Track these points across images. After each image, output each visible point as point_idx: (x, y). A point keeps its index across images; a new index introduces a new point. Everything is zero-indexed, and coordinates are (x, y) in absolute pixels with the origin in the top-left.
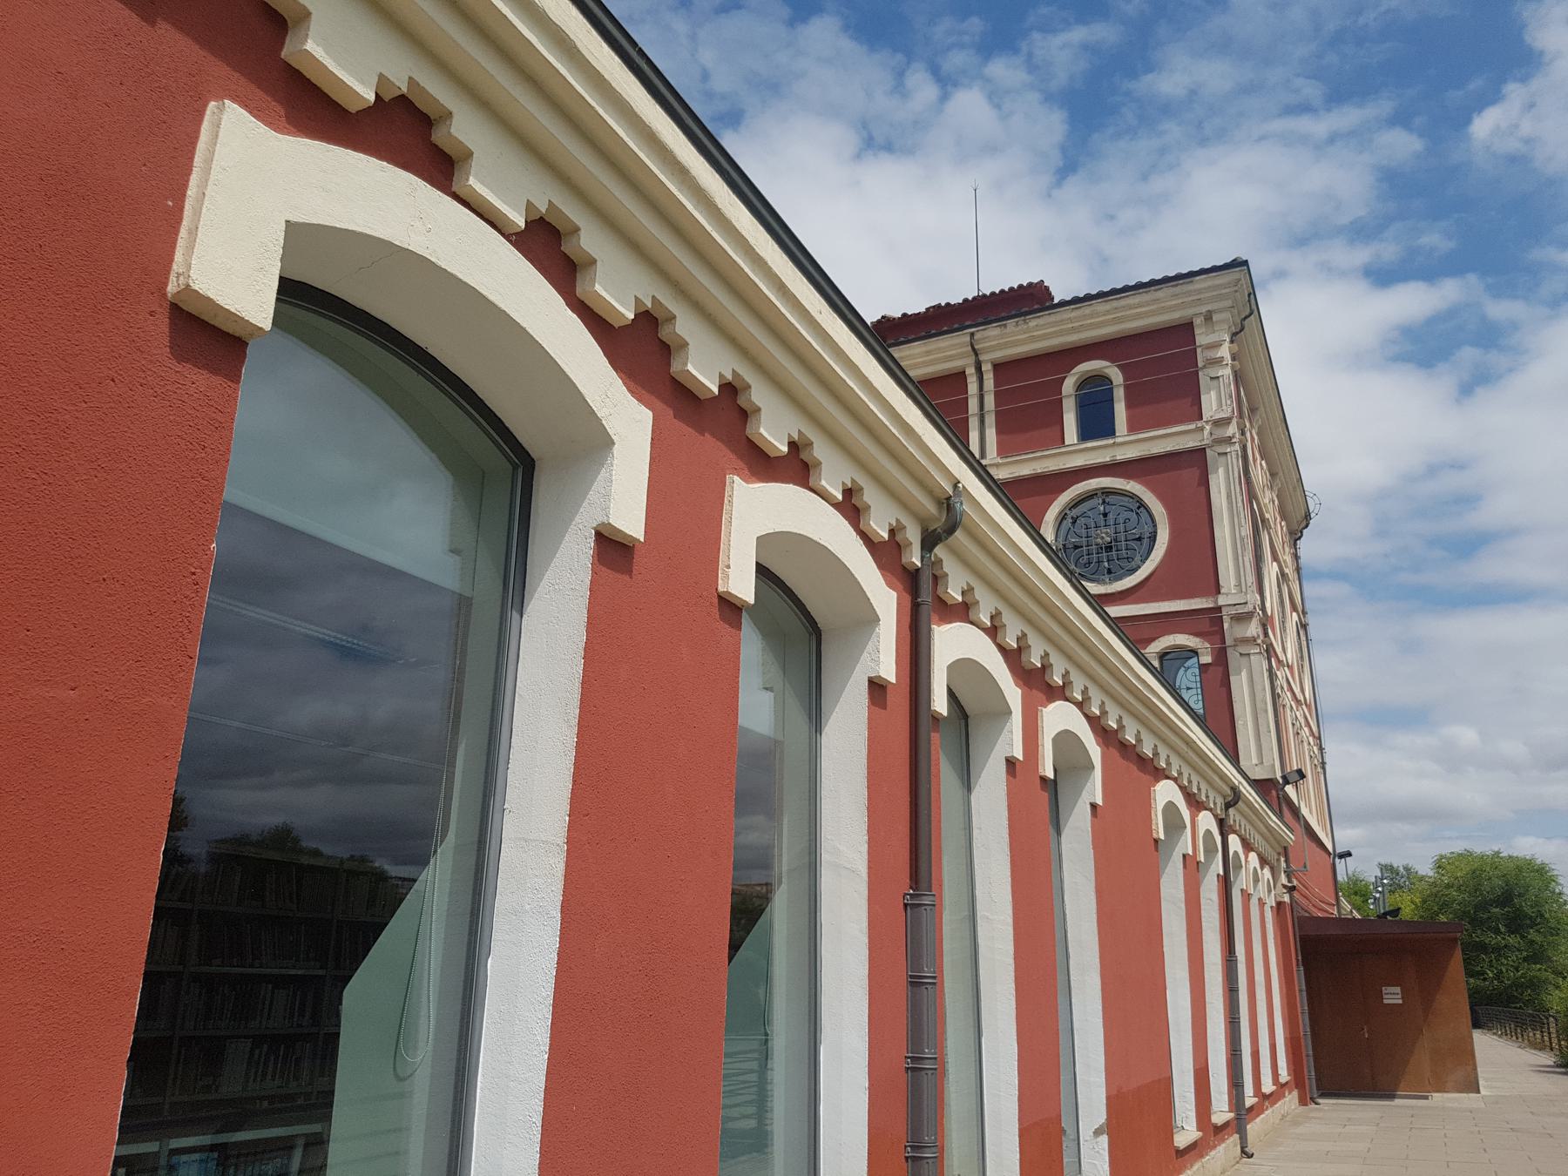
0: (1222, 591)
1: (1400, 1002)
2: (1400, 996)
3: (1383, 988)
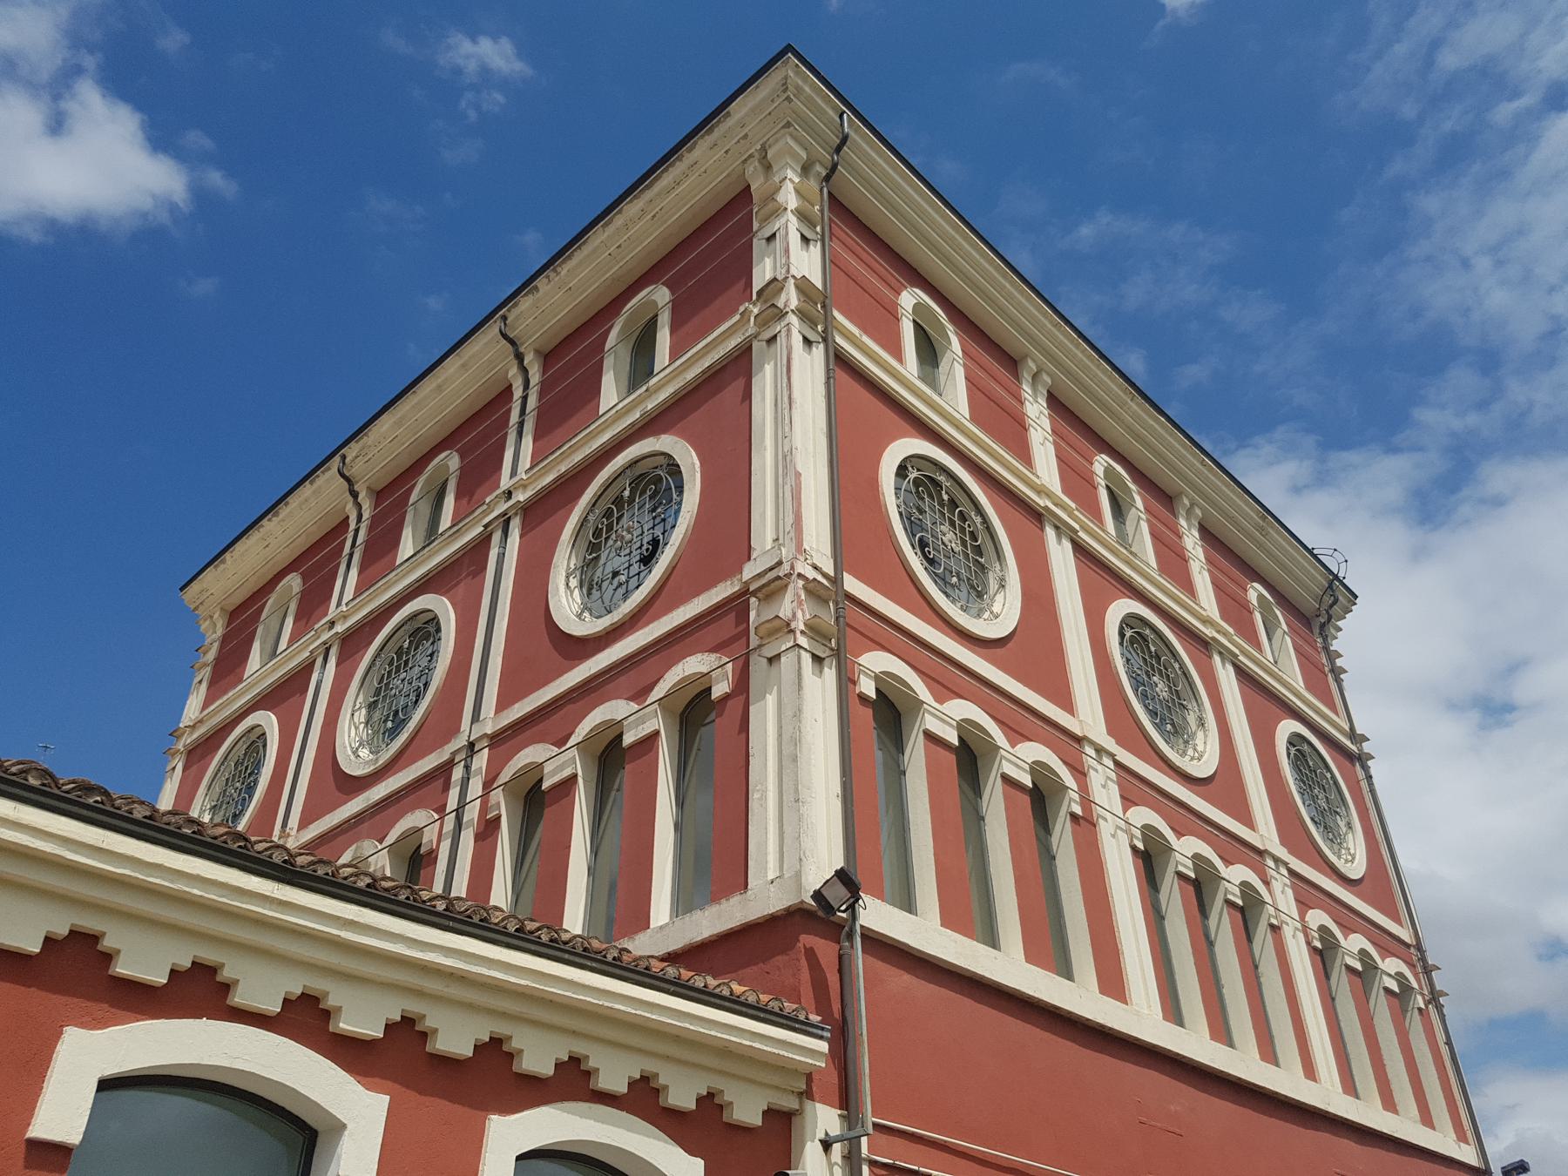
0: (754, 555)
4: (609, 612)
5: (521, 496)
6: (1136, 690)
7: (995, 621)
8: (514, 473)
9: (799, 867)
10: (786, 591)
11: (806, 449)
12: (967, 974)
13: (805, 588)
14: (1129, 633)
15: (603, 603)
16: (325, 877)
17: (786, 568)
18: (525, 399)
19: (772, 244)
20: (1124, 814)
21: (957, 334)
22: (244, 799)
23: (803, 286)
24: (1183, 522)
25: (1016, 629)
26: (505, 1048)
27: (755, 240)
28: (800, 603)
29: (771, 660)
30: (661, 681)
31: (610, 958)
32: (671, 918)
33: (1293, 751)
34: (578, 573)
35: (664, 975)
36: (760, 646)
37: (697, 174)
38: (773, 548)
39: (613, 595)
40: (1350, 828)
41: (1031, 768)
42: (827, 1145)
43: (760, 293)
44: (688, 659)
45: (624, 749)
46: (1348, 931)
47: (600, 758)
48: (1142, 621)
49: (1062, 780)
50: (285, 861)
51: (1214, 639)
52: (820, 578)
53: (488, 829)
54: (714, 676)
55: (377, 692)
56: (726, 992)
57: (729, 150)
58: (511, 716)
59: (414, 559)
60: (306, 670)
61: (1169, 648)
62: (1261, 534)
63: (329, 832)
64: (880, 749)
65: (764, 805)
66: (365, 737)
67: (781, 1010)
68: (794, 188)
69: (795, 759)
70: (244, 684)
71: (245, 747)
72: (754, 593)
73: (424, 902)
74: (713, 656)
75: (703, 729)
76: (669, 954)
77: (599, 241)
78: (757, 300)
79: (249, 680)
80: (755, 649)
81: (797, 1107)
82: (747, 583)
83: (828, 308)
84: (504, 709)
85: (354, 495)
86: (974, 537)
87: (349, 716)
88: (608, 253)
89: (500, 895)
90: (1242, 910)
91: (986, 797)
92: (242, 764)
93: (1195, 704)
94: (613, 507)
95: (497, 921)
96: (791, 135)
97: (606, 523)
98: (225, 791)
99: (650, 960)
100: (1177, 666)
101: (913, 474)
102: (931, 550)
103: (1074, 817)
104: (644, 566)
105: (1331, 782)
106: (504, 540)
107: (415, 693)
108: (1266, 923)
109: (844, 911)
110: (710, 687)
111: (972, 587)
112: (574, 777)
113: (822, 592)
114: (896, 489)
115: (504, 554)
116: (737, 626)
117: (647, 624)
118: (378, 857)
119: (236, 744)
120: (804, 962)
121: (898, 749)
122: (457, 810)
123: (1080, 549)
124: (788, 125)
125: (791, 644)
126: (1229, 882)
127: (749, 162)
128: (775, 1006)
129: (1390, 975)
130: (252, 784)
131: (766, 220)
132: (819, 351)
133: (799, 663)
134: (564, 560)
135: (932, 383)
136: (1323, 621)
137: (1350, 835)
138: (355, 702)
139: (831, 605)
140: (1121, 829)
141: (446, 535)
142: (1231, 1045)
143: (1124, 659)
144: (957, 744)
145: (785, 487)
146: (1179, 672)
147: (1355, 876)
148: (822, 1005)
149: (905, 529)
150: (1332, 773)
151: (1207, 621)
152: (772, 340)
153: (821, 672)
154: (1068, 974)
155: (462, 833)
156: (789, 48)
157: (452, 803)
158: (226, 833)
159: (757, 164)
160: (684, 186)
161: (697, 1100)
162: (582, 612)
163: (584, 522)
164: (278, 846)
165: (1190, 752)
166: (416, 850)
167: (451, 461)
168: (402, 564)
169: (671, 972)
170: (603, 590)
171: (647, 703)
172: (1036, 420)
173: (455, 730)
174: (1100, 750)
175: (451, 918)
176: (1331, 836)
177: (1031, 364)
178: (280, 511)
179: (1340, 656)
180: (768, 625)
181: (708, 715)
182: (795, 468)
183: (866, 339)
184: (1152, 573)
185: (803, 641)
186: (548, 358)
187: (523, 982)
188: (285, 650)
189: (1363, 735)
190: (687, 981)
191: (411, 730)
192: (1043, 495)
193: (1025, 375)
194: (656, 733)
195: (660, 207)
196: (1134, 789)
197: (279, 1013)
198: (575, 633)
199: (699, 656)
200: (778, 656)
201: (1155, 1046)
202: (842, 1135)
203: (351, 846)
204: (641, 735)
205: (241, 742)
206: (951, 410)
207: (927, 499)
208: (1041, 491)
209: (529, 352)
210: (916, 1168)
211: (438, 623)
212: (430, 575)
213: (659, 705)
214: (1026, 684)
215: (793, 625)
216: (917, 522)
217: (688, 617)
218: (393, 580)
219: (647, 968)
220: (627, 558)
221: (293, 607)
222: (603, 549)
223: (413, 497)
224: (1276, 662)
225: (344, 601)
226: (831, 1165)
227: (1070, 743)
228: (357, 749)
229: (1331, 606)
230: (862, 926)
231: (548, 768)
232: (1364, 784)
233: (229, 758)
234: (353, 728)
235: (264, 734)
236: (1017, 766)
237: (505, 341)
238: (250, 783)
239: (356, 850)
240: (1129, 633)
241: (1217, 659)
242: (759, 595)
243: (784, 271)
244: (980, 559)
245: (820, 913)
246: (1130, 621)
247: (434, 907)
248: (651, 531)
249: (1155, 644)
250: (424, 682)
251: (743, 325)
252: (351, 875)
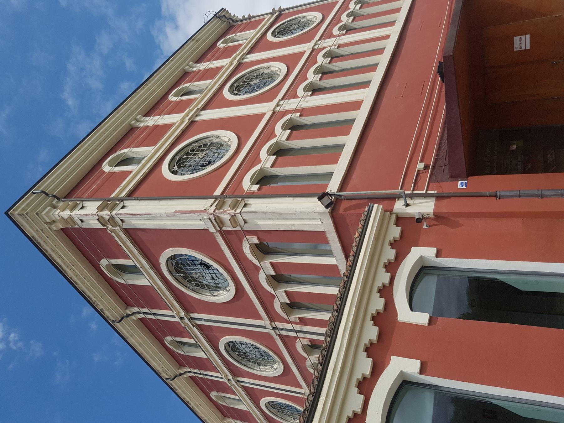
0: (206, 228)
1: (528, 36)
2: (523, 37)
3: (515, 50)
4: (227, 280)
5: (182, 314)
6: (257, 91)
7: (232, 140)
8: (174, 317)
9: (317, 213)
10: (219, 216)
11: (166, 208)
12: (353, 156)
13: (219, 210)
14: (236, 92)
15: (223, 282)
16: (318, 381)
17: (212, 217)
18: (144, 313)
19: (84, 220)
20: (299, 98)
21: (121, 150)
22: (291, 408)
23: (100, 209)
24: (195, 69)
25: (234, 133)
26: (375, 315)
27: (82, 227)
28: (225, 211)
29: (245, 222)
30: (252, 261)
31: (346, 279)
32: (334, 257)
33: (278, 36)
34: (212, 292)
35: (352, 260)
36: (240, 226)
37: (57, 249)
38: (204, 221)
39: (220, 279)
40: (305, 17)
41: (284, 130)
42: (407, 205)
43: (103, 225)
44: (244, 252)
45: (276, 275)
46: (340, 21)
47: (279, 283)
48: (231, 87)
49: (288, 120)
50: (313, 396)
51: (238, 61)
52: (215, 204)
53: (303, 321)
54: (251, 243)
55: (254, 362)
56: (358, 239)
57: (47, 236)
58: (264, 315)
59: (205, 352)
60: (245, 389)
61: (241, 78)
62: (199, 41)
63: (303, 377)
64: (277, 183)
65: (296, 225)
66: (270, 366)
67: (364, 220)
68: (62, 212)
69: (281, 214)
70: (250, 410)
71: (273, 409)
72: (221, 228)
73: (327, 345)
74: (244, 243)
75: (269, 246)
76: (345, 258)
77: (82, 286)
78: (106, 226)
79: (249, 409)
80: (241, 228)
81: (395, 215)
82: (217, 231)
83: (110, 199)
84: (262, 318)
85: (181, 374)
86: (200, 147)
87: (262, 373)
88: (87, 283)
89: (326, 316)
90: (332, 58)
91: (294, 147)
92: (279, 410)
93: (261, 70)
94: (187, 280)
95: (334, 319)
96: (41, 212)
97: (193, 282)
98: (288, 415)
99: (347, 265)
100: (248, 75)
101: (176, 168)
102: (205, 163)
103: (300, 116)
104: (210, 268)
105: (289, 23)
106: (199, 319)
107: (255, 349)
108: (337, 50)
109: (332, 198)
110: (255, 244)
111: (219, 148)
112: (285, 292)
113: (221, 203)
114: (181, 175)
115: (204, 319)
116: (233, 235)
117: (232, 267)
118: (312, 360)
119: (272, 413)
120: (348, 212)
121: (277, 177)
122: (296, 333)
123: (204, 108)
124: (37, 214)
125: (240, 215)
126: (323, 62)
127: (51, 229)
128: (362, 222)
129: (355, 7)
130: (286, 406)
131: (74, 223)
132: (127, 203)
133: (246, 212)
134: (207, 297)
135: (140, 160)
136: (231, 21)
137: (307, 17)
138: (258, 370)
139: (225, 200)
140: (305, 99)
141: (197, 340)
142: (377, 64)
143: (245, 94)
144: (276, 156)
145: (180, 216)
146: (250, 74)
147: (321, 17)
148: (363, 206)
149: (197, 172)
150: (286, 22)
151: (231, 63)
152: (122, 221)
153: (250, 204)
154: (353, 121)
155: (304, 330)
156: (6, 213)
157: (294, 334)
158: (303, 418)
159: (52, 226)
160: (61, 254)
161: (393, 249)
162: (227, 290)
163: (193, 290)
164: (308, 397)
165: (278, 73)
166: (310, 347)
167: (168, 339)
168: (207, 356)
169: (351, 258)
170: (219, 283)
171: (260, 266)
172: (155, 121)
173: (268, 334)
174: (278, 105)
175: (333, 335)
176: (307, 24)
178: (187, 401)
179: (244, 16)
180: (233, 223)
181: (265, 244)
182: (173, 213)
183: (122, 185)
184: (214, 82)
185: (238, 211)
186: (128, 305)
187: (354, 310)
188: (238, 396)
189: (272, 10)
190: (354, 252)
191: (268, 350)
192: (184, 120)
193: (137, 125)
194: (271, 263)
195: (69, 263)
196: (291, 94)
197: (364, 396)
198: (234, 293)
199: (243, 248)
200: (244, 219)
201: (377, 91)
202: (404, 200)
203: (308, 369)
204: (272, 268)
205: (271, 410)
206: (151, 153)
207: (186, 164)
208: (182, 121)
209: (126, 312)
210: (415, 175)
211: (229, 342)
212: (212, 346)
213: (261, 262)
215: (233, 214)
216: (194, 168)
217: (229, 252)
218: (214, 359)
219: (350, 266)
220: (207, 274)
221: (222, 394)
222: (203, 283)
223: (182, 353)
224: (246, 39)
225: (221, 376)
226: (414, 204)
227: (275, 116)
228: (274, 369)
229: (226, 18)
230: (337, 192)
231: (283, 301)
232: (290, 11)
233: (277, 414)
234: (267, 371)
235: (268, 402)
236: (283, 135)
237: (122, 321)
238: (286, 406)
239: (309, 368)
240: (236, 92)
241: (245, 60)
242: (221, 226)
243: (95, 216)
244: (209, 145)
245: (333, 206)
246: (231, 91)
247: (329, 341)
248: (197, 265)
249: (240, 83)
250: (251, 346)
251: (116, 231)
252: (318, 372)
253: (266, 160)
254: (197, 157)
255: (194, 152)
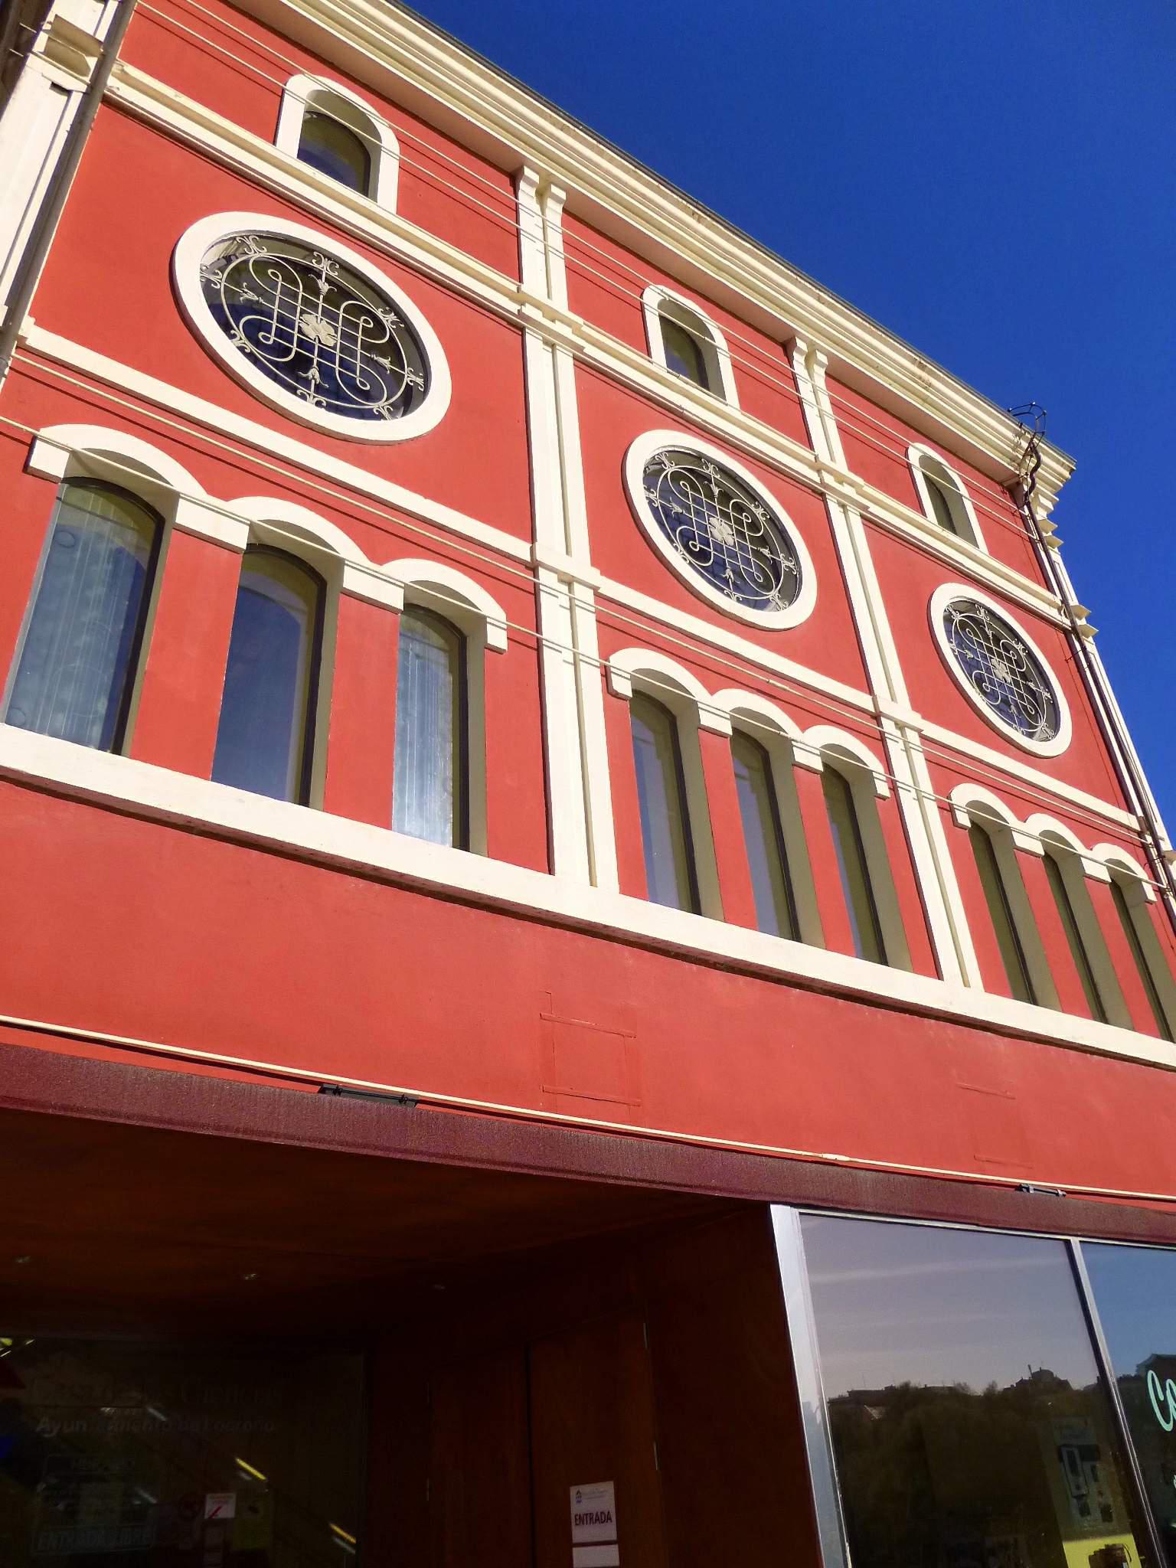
2: (610, 1531)
150: (1024, 643)
177: (800, 344)
214: (427, 495)
229: (1035, 469)
253: (716, 712)
254: (995, 660)
255: (994, 648)
